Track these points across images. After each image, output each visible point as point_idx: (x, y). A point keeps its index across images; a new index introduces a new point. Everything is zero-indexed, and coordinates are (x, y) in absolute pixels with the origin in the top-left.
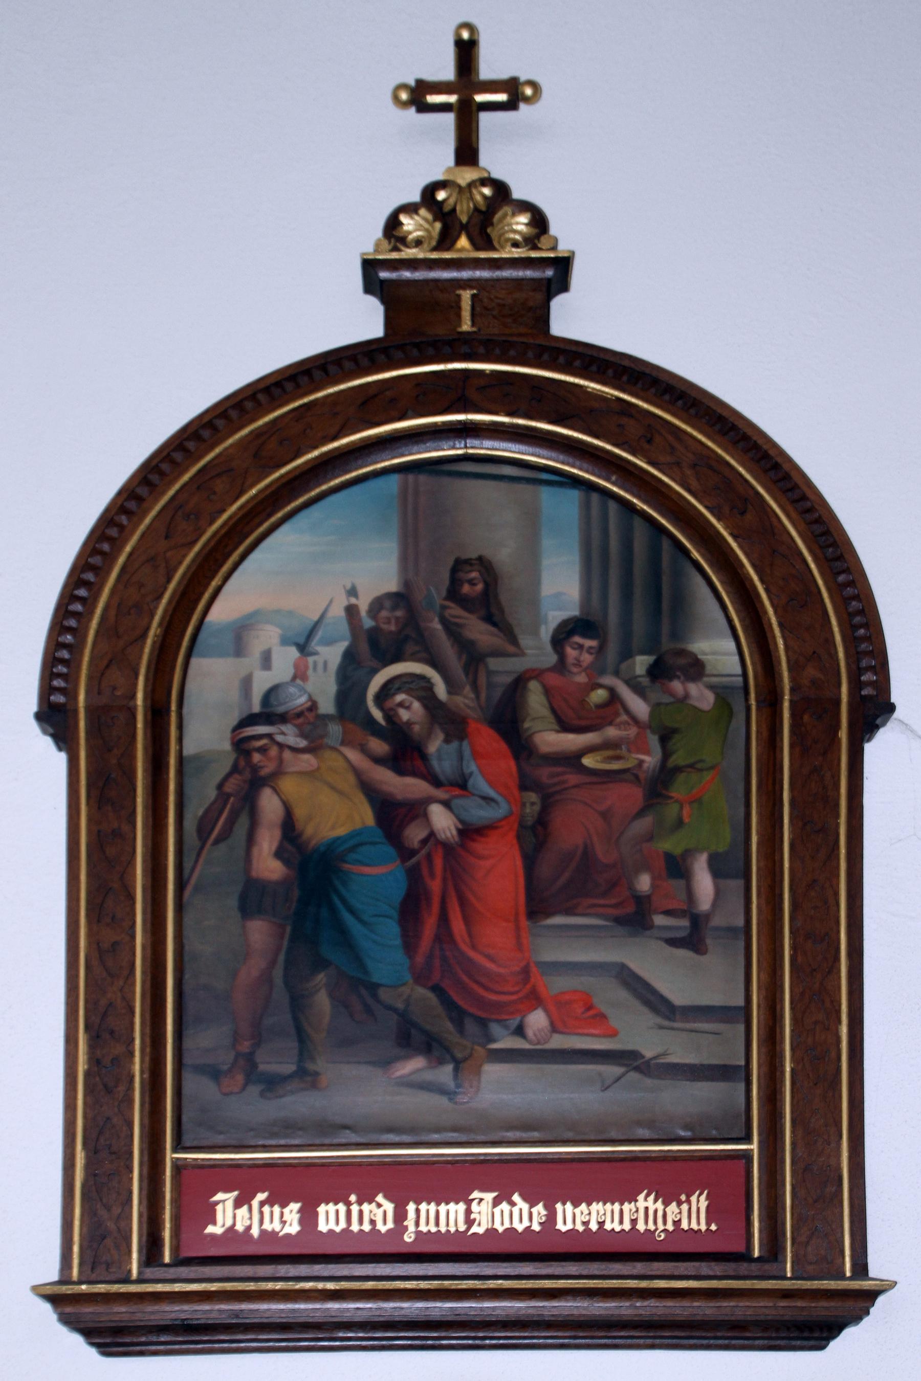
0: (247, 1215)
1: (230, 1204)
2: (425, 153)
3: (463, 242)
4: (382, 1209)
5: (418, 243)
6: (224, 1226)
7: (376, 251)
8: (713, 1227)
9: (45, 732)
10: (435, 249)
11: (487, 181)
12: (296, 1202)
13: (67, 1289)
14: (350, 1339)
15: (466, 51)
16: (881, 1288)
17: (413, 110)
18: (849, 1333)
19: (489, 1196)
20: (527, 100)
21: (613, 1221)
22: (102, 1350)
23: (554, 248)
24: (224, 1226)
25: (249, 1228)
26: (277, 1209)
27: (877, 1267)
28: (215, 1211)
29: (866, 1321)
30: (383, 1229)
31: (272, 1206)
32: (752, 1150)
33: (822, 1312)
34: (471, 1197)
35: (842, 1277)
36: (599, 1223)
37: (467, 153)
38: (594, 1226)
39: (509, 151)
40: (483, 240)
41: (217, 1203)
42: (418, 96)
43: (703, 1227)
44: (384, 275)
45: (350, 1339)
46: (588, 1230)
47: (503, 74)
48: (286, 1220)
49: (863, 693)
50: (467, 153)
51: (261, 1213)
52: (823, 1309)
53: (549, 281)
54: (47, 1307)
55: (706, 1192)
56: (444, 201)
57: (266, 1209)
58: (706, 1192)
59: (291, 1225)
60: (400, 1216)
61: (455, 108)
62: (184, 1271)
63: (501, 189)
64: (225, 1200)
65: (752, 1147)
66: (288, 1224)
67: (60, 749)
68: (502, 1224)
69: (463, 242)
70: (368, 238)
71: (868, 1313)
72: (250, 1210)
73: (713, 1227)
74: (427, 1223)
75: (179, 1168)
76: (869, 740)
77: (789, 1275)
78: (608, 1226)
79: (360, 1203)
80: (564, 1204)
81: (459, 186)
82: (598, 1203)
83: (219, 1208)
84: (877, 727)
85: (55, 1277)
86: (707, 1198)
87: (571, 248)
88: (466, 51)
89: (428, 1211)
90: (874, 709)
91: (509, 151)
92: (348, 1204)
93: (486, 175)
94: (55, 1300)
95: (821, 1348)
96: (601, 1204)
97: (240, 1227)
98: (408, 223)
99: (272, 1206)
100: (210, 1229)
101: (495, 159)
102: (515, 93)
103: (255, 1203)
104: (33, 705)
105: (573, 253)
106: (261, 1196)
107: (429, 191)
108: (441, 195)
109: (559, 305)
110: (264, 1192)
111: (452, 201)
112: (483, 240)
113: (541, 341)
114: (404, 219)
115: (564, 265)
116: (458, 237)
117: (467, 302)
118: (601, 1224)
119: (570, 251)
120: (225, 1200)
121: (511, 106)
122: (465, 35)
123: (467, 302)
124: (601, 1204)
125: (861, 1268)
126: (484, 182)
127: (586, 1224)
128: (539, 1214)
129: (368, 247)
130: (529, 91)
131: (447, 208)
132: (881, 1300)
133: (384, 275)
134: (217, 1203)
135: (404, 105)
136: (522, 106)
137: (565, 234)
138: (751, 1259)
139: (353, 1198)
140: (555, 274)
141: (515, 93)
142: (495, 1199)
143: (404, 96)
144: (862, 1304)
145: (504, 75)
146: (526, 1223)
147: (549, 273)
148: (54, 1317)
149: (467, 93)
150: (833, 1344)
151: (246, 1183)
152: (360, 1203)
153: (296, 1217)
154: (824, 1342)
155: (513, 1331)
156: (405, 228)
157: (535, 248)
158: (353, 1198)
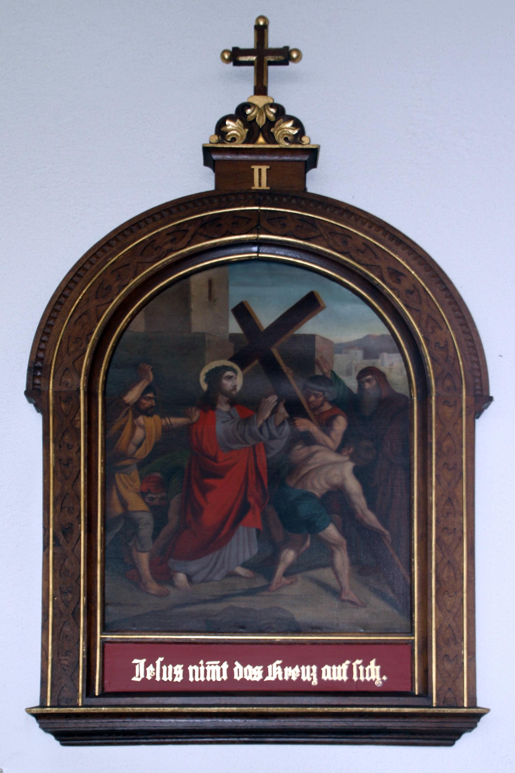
0: (299, 671)
2: (238, 87)
3: (261, 140)
5: (233, 140)
6: (272, 676)
7: (211, 143)
8: (385, 678)
10: (243, 143)
11: (273, 105)
12: (180, 664)
15: (261, 31)
17: (231, 64)
18: (466, 737)
19: (142, 662)
20: (294, 60)
24: (139, 677)
25: (155, 677)
28: (135, 668)
29: (475, 731)
31: (167, 666)
37: (261, 89)
39: (285, 88)
40: (270, 138)
41: (136, 664)
42: (235, 56)
44: (215, 157)
48: (175, 673)
50: (261, 89)
51: (358, 671)
52: (455, 724)
53: (306, 162)
54: (33, 719)
57: (164, 668)
59: (179, 676)
60: (230, 672)
62: (103, 701)
63: (280, 111)
64: (140, 663)
65: (413, 638)
69: (261, 140)
70: (207, 135)
72: (155, 666)
75: (104, 643)
76: (478, 417)
77: (434, 705)
84: (483, 411)
85: (38, 704)
87: (318, 143)
88: (261, 31)
90: (482, 399)
91: (285, 88)
92: (199, 666)
93: (271, 101)
94: (38, 717)
95: (452, 745)
97: (149, 677)
98: (230, 125)
100: (134, 679)
102: (285, 56)
103: (158, 662)
104: (23, 387)
105: (319, 146)
106: (161, 659)
107: (242, 109)
108: (249, 111)
109: (311, 174)
111: (254, 113)
114: (227, 122)
115: (313, 154)
116: (257, 138)
117: (260, 175)
120: (140, 663)
121: (285, 63)
122: (261, 23)
123: (260, 175)
129: (206, 142)
130: (294, 55)
131: (249, 118)
132: (483, 719)
133: (215, 157)
135: (228, 61)
136: (291, 63)
137: (312, 137)
138: (414, 695)
139: (201, 662)
140: (309, 159)
141: (285, 56)
143: (226, 56)
147: (306, 158)
148: (37, 725)
149: (262, 56)
150: (458, 743)
151: (150, 652)
154: (451, 742)
156: (229, 127)
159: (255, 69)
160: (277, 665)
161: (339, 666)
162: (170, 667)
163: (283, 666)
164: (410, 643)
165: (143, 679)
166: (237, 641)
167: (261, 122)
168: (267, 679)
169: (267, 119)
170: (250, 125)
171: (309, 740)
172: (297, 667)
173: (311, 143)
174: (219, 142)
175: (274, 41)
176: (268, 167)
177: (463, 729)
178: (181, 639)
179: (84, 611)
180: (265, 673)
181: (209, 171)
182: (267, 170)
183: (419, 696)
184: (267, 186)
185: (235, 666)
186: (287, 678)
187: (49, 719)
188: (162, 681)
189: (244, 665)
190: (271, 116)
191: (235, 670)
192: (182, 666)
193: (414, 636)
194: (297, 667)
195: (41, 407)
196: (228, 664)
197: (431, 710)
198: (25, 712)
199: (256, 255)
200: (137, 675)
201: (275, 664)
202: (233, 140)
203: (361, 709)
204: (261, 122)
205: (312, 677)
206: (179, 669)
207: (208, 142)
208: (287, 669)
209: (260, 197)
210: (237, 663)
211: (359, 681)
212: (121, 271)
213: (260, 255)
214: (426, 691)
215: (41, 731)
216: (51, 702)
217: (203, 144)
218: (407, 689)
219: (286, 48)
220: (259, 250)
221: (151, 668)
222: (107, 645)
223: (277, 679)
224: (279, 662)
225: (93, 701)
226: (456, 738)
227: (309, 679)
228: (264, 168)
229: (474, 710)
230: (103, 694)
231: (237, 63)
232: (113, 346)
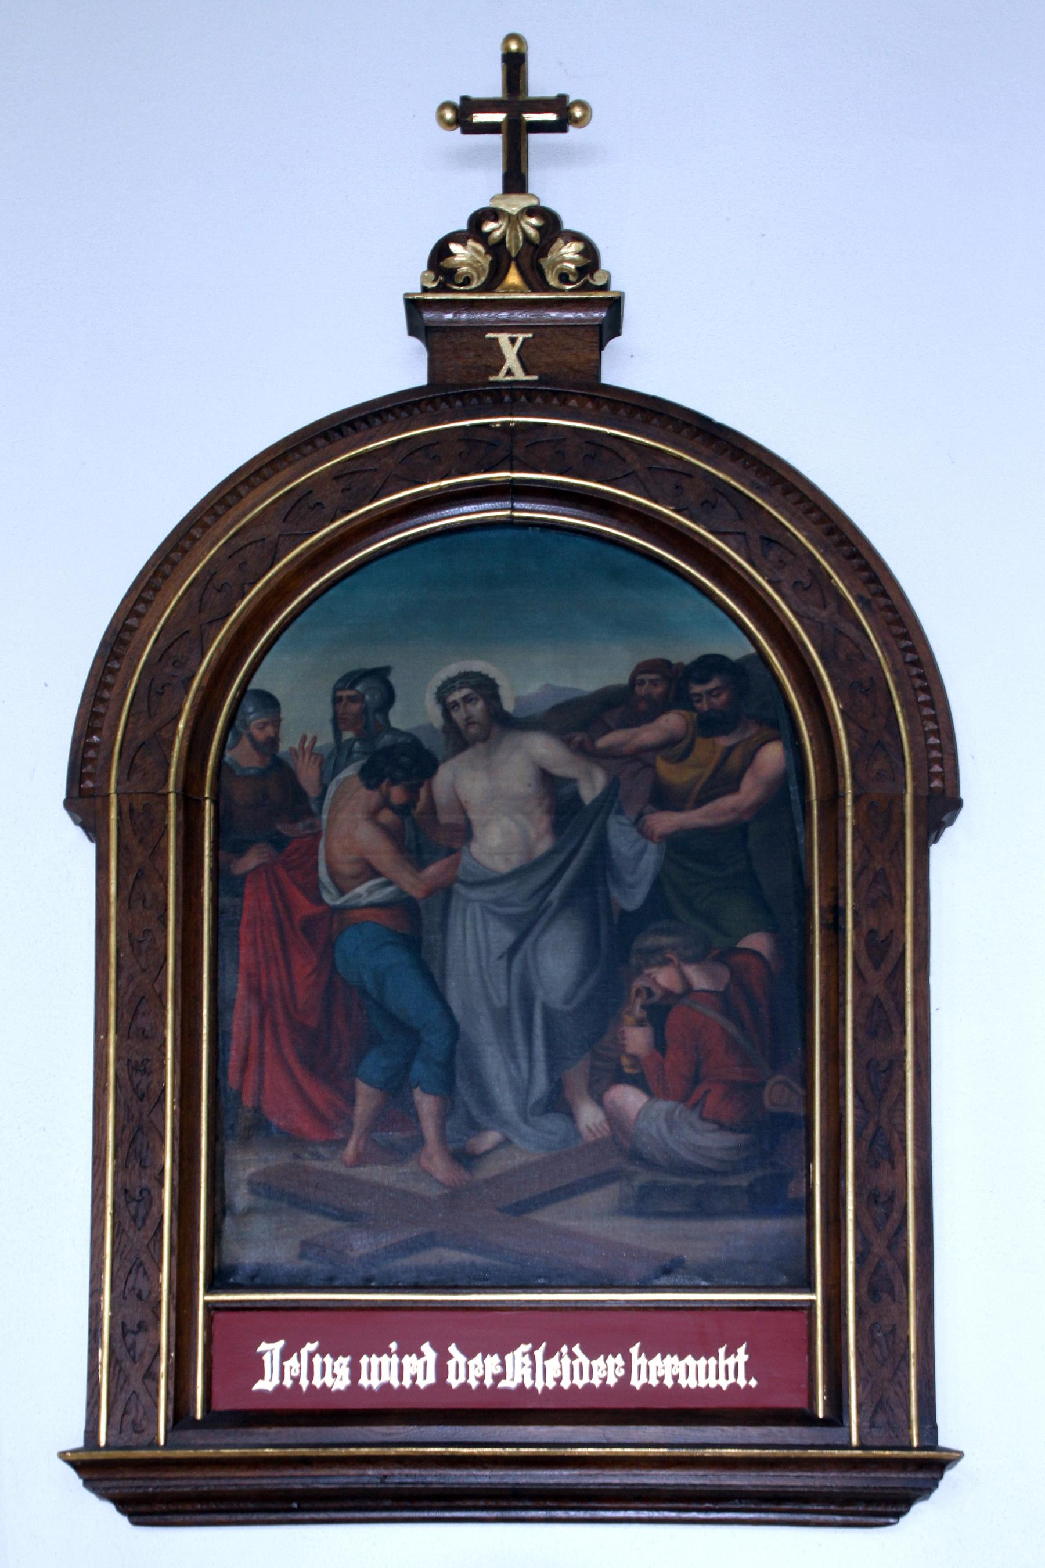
3: (513, 278)
4: (423, 1360)
6: (513, 1379)
7: (425, 290)
8: (753, 1383)
9: (76, 823)
15: (514, 64)
18: (920, 1510)
21: (707, 1376)
22: (136, 1519)
23: (605, 288)
24: (513, 1379)
26: (328, 1359)
27: (946, 1439)
29: (936, 1495)
30: (422, 1384)
31: (323, 1356)
32: (813, 1302)
34: (259, 1349)
35: (153, 1444)
36: (658, 1378)
37: (515, 179)
38: (669, 1383)
39: (560, 180)
42: (463, 115)
43: (742, 1382)
46: (558, 1388)
49: (932, 786)
50: (515, 179)
55: (544, 1345)
58: (544, 1345)
60: (442, 1370)
61: (504, 128)
63: (551, 223)
64: (271, 1350)
65: (209, 1298)
66: (338, 1377)
67: (92, 841)
69: (513, 278)
70: (413, 276)
71: (937, 1486)
73: (753, 1383)
74: (323, 1374)
76: (936, 841)
77: (915, 1444)
78: (566, 1384)
79: (401, 1356)
81: (509, 216)
82: (672, 1356)
83: (266, 1358)
85: (80, 1443)
86: (746, 1352)
88: (514, 64)
89: (707, 1367)
90: (942, 805)
91: (560, 180)
93: (534, 202)
96: (676, 1357)
99: (323, 1356)
102: (564, 114)
103: (304, 1353)
106: (311, 1347)
107: (478, 219)
108: (488, 227)
110: (527, 1343)
112: (535, 278)
114: (454, 248)
115: (615, 305)
117: (515, 338)
118: (675, 1378)
121: (559, 127)
122: (514, 46)
123: (515, 338)
124: (676, 1357)
126: (531, 211)
127: (481, 1379)
130: (578, 113)
132: (949, 1475)
133: (428, 315)
135: (449, 125)
136: (571, 128)
137: (619, 270)
139: (722, 1351)
141: (564, 114)
143: (449, 115)
144: (935, 1475)
145: (551, 93)
146: (462, 1379)
147: (600, 315)
149: (517, 115)
151: (295, 1326)
157: (587, 287)
158: (393, 1346)
160: (524, 1354)
161: (703, 1359)
164: (803, 1308)
165: (348, 1388)
166: (357, 1304)
167: (513, 246)
169: (527, 238)
170: (497, 249)
171: (656, 1514)
175: (540, 83)
176: (530, 335)
177: (918, 1493)
181: (416, 345)
183: (825, 1422)
185: (451, 1357)
186: (407, 1383)
187: (824, 1470)
188: (402, 1387)
189: (470, 1355)
190: (532, 232)
191: (451, 1364)
195: (92, 825)
199: (508, 513)
203: (497, 1450)
204: (513, 246)
206: (342, 1365)
207: (419, 290)
209: (511, 397)
210: (453, 1349)
211: (311, 1387)
213: (516, 514)
214: (837, 1416)
217: (406, 294)
219: (562, 98)
221: (293, 1361)
222: (219, 1316)
223: (522, 1386)
225: (190, 1434)
226: (903, 1509)
230: (215, 1419)
232: (234, 698)
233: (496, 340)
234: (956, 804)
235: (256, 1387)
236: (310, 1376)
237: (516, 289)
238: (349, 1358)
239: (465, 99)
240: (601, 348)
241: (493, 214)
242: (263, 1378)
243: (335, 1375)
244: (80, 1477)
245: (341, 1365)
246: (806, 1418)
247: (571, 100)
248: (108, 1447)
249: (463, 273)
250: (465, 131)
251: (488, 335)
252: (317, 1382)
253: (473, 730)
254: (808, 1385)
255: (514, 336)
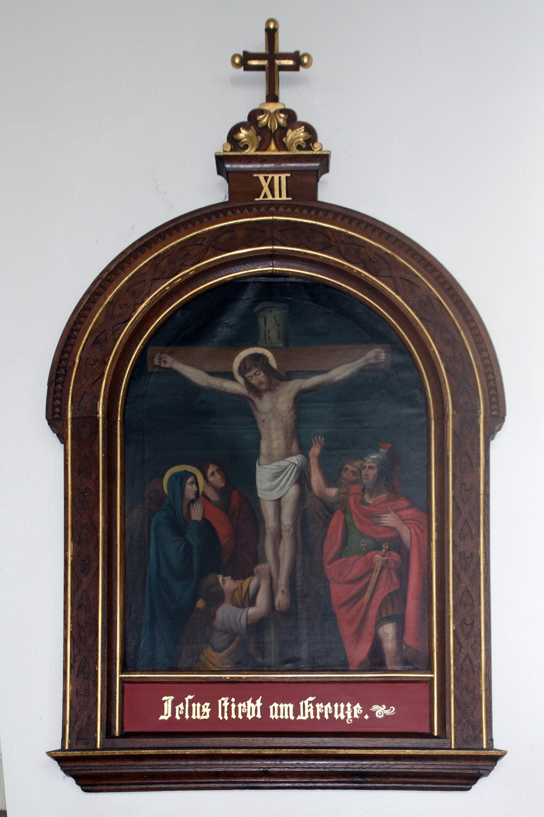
0: (182, 708)
1: (170, 701)
2: (250, 95)
3: (273, 146)
7: (224, 151)
9: (54, 432)
13: (305, 752)
14: (246, 782)
15: (271, 34)
16: (499, 754)
18: (482, 783)
20: (304, 65)
22: (85, 788)
33: (465, 765)
37: (272, 97)
41: (165, 701)
42: (245, 61)
45: (318, 782)
47: (291, 50)
50: (272, 97)
54: (56, 763)
56: (260, 120)
62: (122, 742)
63: (291, 115)
64: (168, 700)
68: (251, 715)
69: (273, 146)
70: (220, 144)
71: (493, 769)
72: (184, 706)
74: (274, 714)
75: (122, 680)
76: (492, 439)
77: (485, 747)
80: (196, 703)
83: (166, 704)
85: (59, 747)
88: (271, 34)
90: (497, 416)
94: (59, 759)
95: (469, 789)
100: (162, 718)
101: (288, 97)
102: (298, 61)
105: (330, 152)
107: (253, 115)
109: (324, 178)
110: (313, 696)
112: (282, 146)
113: (311, 204)
115: (324, 160)
119: (328, 151)
121: (295, 68)
122: (272, 26)
125: (490, 746)
128: (328, 709)
129: (220, 151)
130: (305, 60)
132: (499, 762)
134: (165, 701)
136: (301, 68)
137: (325, 142)
140: (319, 167)
141: (298, 61)
142: (252, 702)
143: (237, 61)
145: (292, 50)
146: (254, 715)
149: (271, 62)
150: (474, 787)
151: (179, 690)
152: (236, 703)
153: (208, 711)
154: (469, 786)
155: (188, 779)
159: (266, 75)
160: (309, 702)
162: (199, 705)
163: (314, 703)
165: (170, 718)
168: (299, 718)
172: (322, 704)
173: (323, 149)
174: (231, 150)
175: (284, 45)
176: (289, 175)
178: (449, 596)
179: (411, 349)
180: (297, 712)
181: (222, 180)
182: (287, 178)
184: (287, 196)
190: (281, 121)
192: (358, 704)
193: (432, 673)
194: (322, 704)
196: (361, 705)
197: (482, 753)
198: (46, 755)
199: (271, 268)
200: (165, 713)
201: (306, 702)
202: (246, 147)
205: (346, 715)
208: (318, 705)
211: (190, 718)
212: (134, 292)
215: (62, 773)
216: (455, 746)
218: (425, 729)
219: (297, 53)
220: (273, 264)
221: (181, 706)
224: (311, 699)
227: (343, 717)
228: (284, 176)
229: (491, 753)
230: (124, 735)
231: (248, 68)
233: (258, 177)
234: (503, 420)
235: (160, 718)
236: (190, 714)
237: (273, 151)
238: (358, 704)
239: (245, 53)
240: (318, 181)
241: (261, 112)
242: (300, 714)
243: (201, 712)
244: (59, 765)
245: (206, 706)
246: (430, 736)
247: (301, 54)
248: (69, 750)
249: (245, 142)
250: (245, 70)
251: (255, 175)
252: (194, 717)
253: (263, 387)
254: (123, 721)
255: (266, 175)
